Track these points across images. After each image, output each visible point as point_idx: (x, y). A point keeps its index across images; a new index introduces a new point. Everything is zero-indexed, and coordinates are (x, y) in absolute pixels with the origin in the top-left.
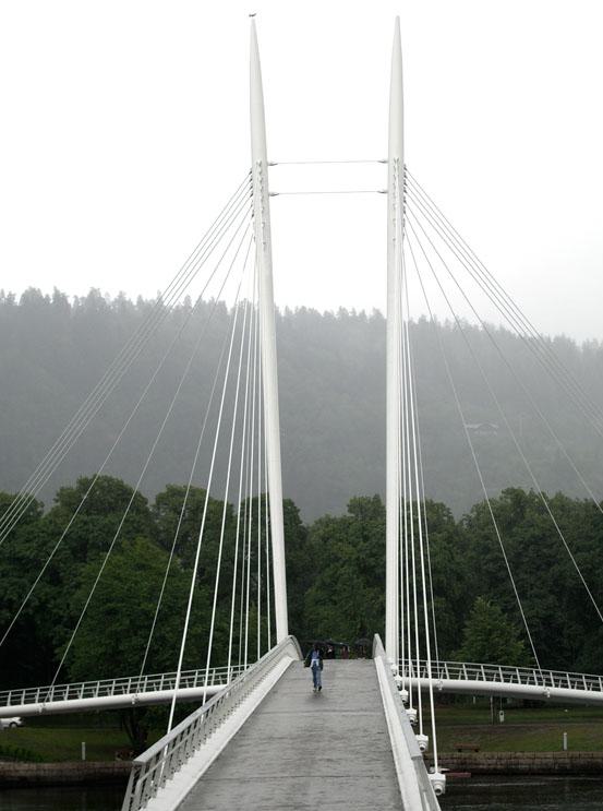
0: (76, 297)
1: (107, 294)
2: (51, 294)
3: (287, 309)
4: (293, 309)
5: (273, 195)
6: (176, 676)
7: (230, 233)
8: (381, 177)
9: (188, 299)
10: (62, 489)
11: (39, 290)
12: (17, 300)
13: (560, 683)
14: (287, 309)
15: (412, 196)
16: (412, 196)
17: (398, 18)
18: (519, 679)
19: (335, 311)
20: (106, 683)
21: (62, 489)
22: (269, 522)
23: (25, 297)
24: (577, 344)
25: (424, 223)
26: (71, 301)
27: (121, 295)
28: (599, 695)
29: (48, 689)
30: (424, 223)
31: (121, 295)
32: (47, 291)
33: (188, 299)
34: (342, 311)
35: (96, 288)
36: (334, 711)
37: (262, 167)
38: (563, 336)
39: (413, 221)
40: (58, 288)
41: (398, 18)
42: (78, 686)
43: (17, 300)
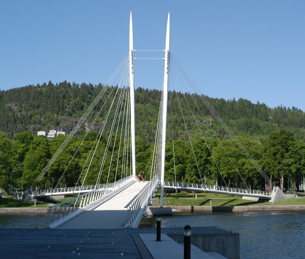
0: (95, 85)
1: (104, 85)
2: (89, 84)
3: (151, 89)
4: (152, 90)
6: (95, 186)
11: (86, 83)
13: (225, 190)
14: (151, 89)
15: (171, 60)
16: (171, 60)
18: (219, 189)
20: (94, 186)
22: (131, 146)
24: (226, 101)
26: (94, 86)
29: (74, 188)
32: (88, 84)
35: (100, 83)
38: (222, 98)
40: (91, 83)
42: (90, 186)
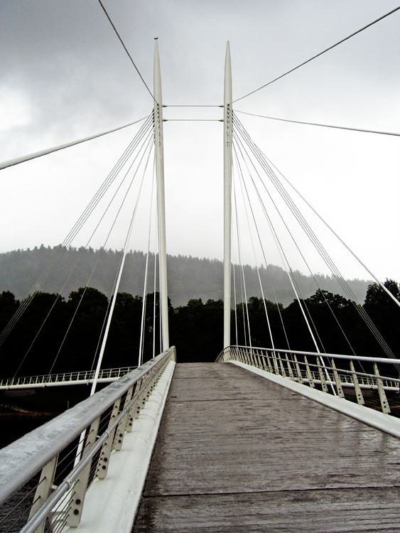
5: (164, 106)
7: (138, 148)
8: (221, 113)
9: (131, 251)
10: (72, 292)
12: (77, 250)
17: (228, 42)
19: (177, 256)
21: (72, 292)
23: (80, 249)
25: (241, 139)
26: (94, 251)
27: (110, 249)
28: (398, 389)
30: (241, 139)
31: (110, 249)
33: (131, 251)
34: (179, 255)
36: (374, 509)
37: (159, 107)
39: (236, 147)
41: (228, 42)
43: (77, 250)
